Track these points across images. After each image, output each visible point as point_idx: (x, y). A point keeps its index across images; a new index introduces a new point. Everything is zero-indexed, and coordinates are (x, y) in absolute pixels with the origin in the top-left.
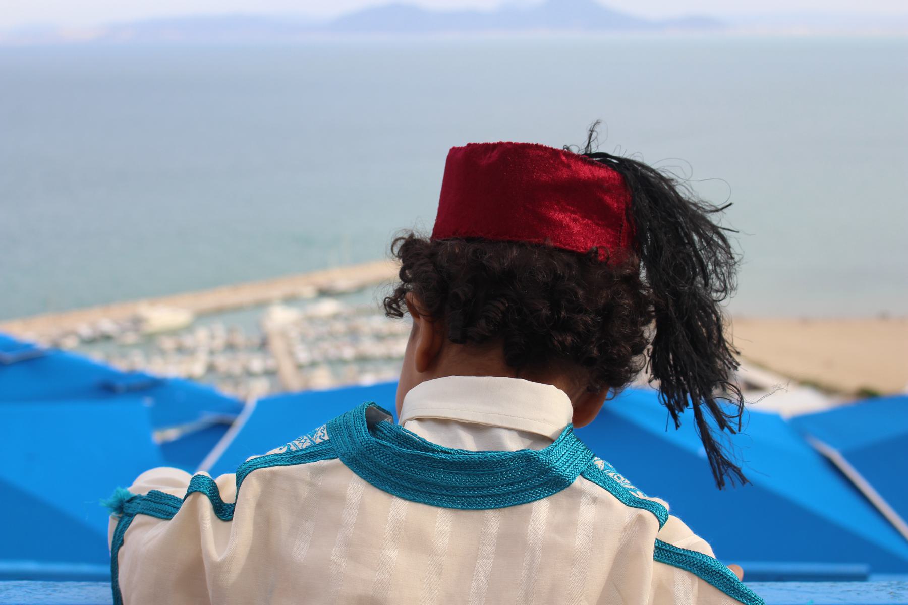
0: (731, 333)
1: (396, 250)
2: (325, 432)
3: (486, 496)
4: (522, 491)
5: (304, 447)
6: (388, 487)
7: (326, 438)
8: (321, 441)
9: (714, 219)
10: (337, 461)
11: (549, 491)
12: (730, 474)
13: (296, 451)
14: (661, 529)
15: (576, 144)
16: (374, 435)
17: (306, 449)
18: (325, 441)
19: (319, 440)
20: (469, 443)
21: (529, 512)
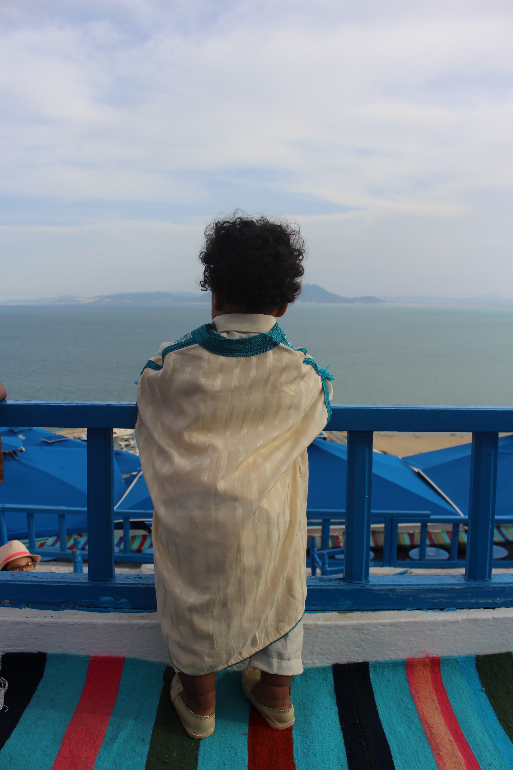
0: (299, 231)
1: (202, 255)
2: (191, 335)
3: (251, 351)
4: (263, 348)
5: (184, 341)
6: (217, 352)
7: (191, 337)
8: (189, 338)
9: (294, 383)
10: (197, 345)
11: (272, 347)
12: (337, 583)
13: (181, 343)
14: (306, 356)
15: (299, 225)
16: (210, 335)
17: (184, 341)
18: (191, 338)
19: (189, 338)
20: (244, 336)
21: (267, 355)
